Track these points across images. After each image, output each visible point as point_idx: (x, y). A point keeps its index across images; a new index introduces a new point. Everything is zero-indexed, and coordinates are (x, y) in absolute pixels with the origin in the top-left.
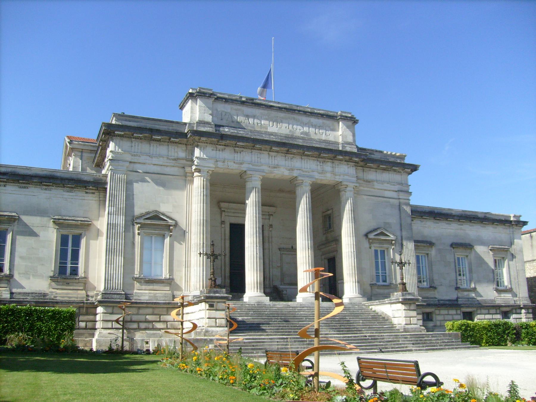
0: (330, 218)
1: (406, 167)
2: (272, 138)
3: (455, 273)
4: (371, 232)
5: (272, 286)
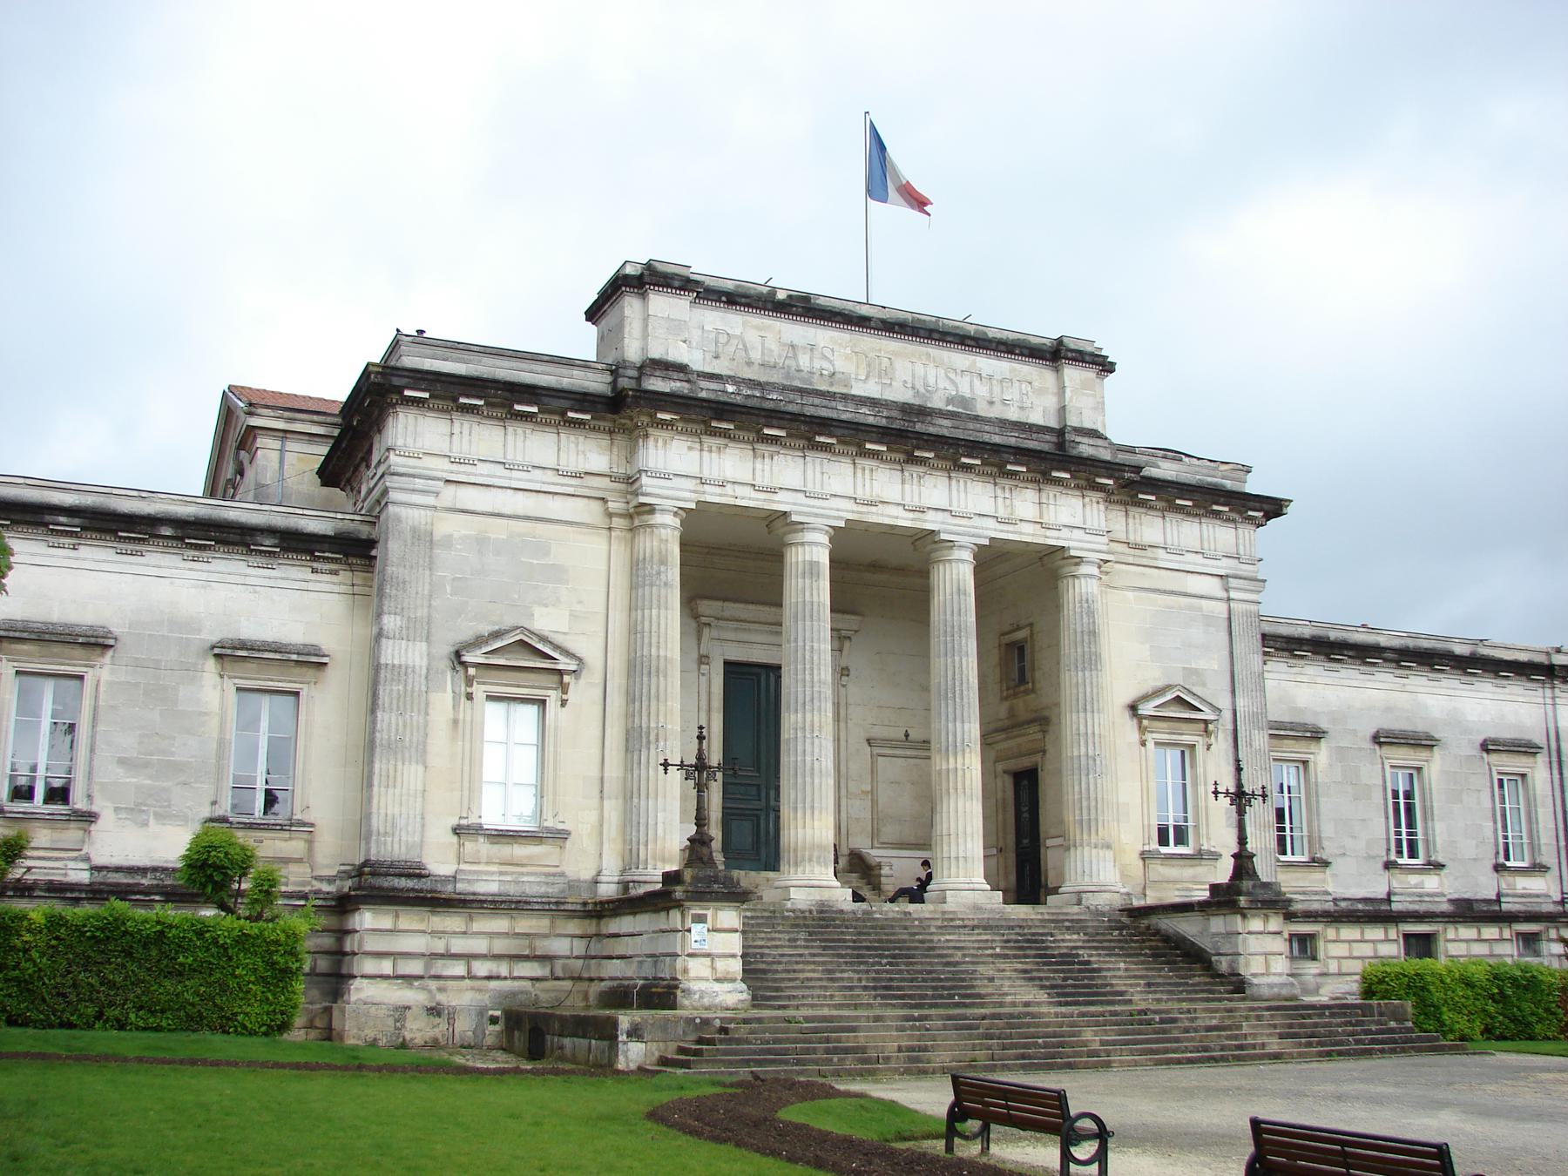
0: (1021, 650)
1: (1251, 504)
2: (867, 416)
4: (1146, 698)
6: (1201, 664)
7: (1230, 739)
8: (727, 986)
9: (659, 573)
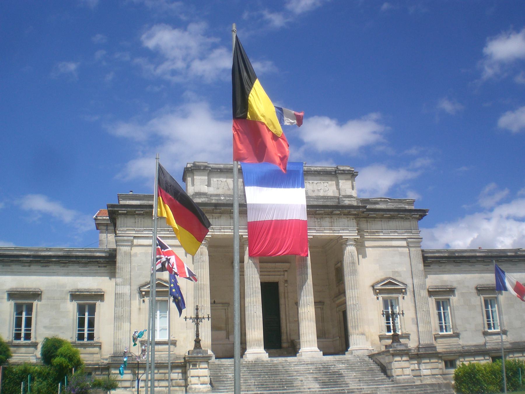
3: (482, 317)
4: (378, 283)
5: (289, 341)
6: (399, 269)
7: (412, 294)
8: (204, 386)
9: (201, 258)
